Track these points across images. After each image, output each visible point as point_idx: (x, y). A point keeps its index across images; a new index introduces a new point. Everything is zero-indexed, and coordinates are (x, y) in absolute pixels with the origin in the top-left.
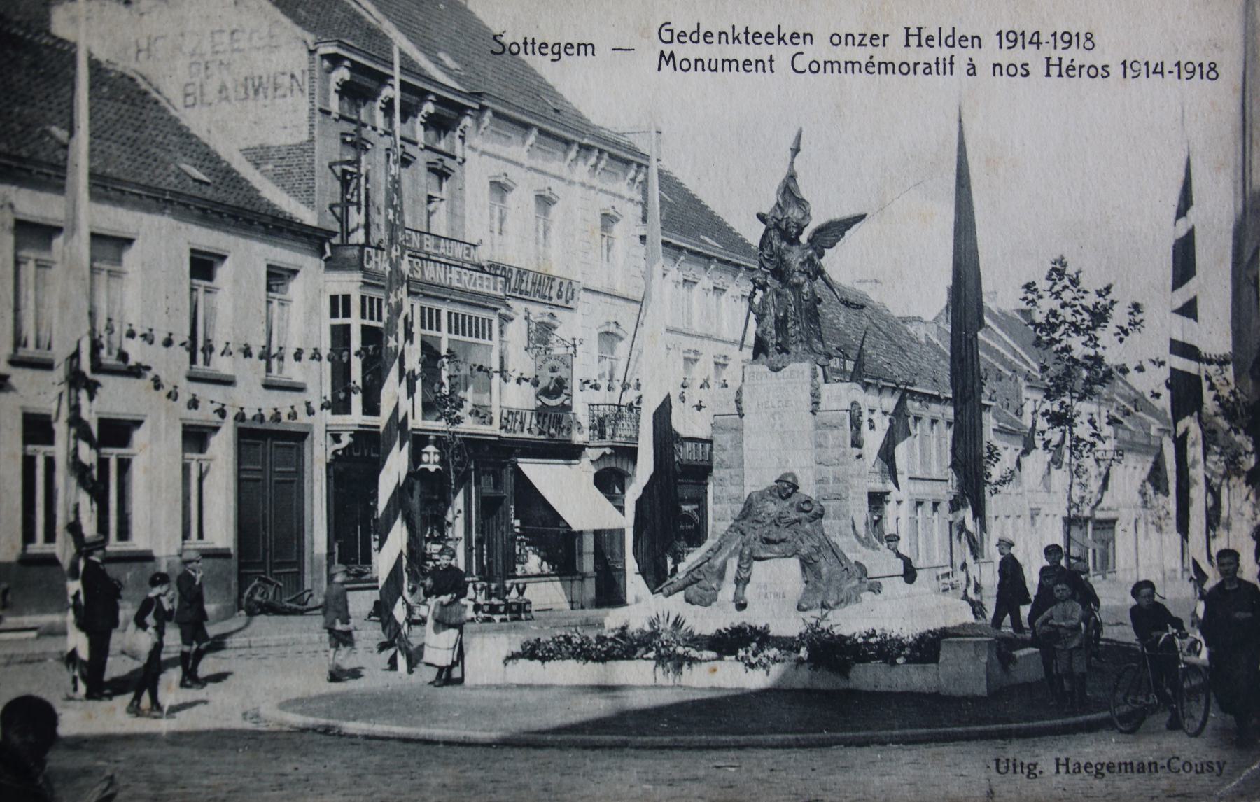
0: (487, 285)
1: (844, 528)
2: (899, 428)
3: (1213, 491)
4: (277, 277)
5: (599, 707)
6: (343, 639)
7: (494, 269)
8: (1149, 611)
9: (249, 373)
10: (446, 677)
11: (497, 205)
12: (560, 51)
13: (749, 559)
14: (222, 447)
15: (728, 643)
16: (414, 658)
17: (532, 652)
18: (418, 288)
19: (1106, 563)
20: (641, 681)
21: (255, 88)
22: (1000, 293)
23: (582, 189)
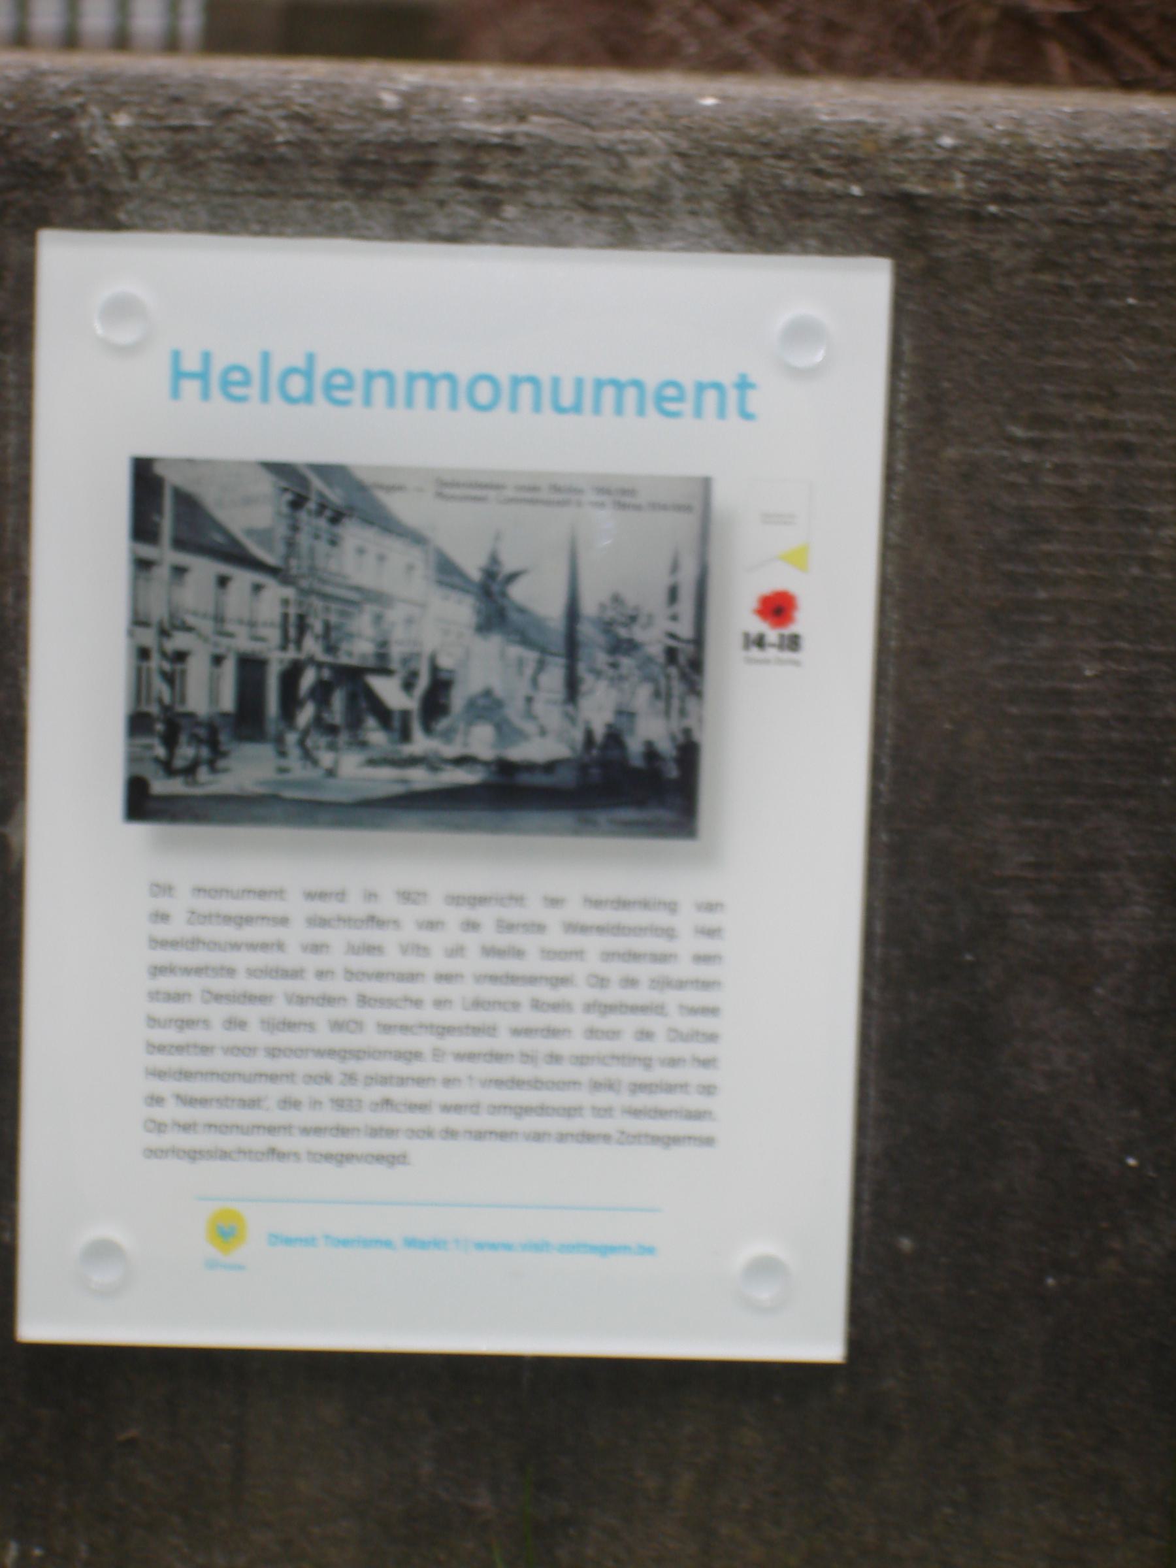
0: (353, 596)
1: (514, 712)
2: (541, 666)
3: (682, 700)
4: (257, 588)
5: (399, 789)
6: (282, 754)
7: (358, 589)
8: (651, 753)
9: (242, 632)
10: (331, 773)
11: (358, 557)
12: (391, 489)
13: (470, 724)
14: (229, 669)
15: (462, 761)
16: (315, 762)
17: (372, 762)
18: (325, 597)
19: (632, 731)
20: (420, 779)
21: (248, 501)
22: (589, 606)
23: (399, 553)
